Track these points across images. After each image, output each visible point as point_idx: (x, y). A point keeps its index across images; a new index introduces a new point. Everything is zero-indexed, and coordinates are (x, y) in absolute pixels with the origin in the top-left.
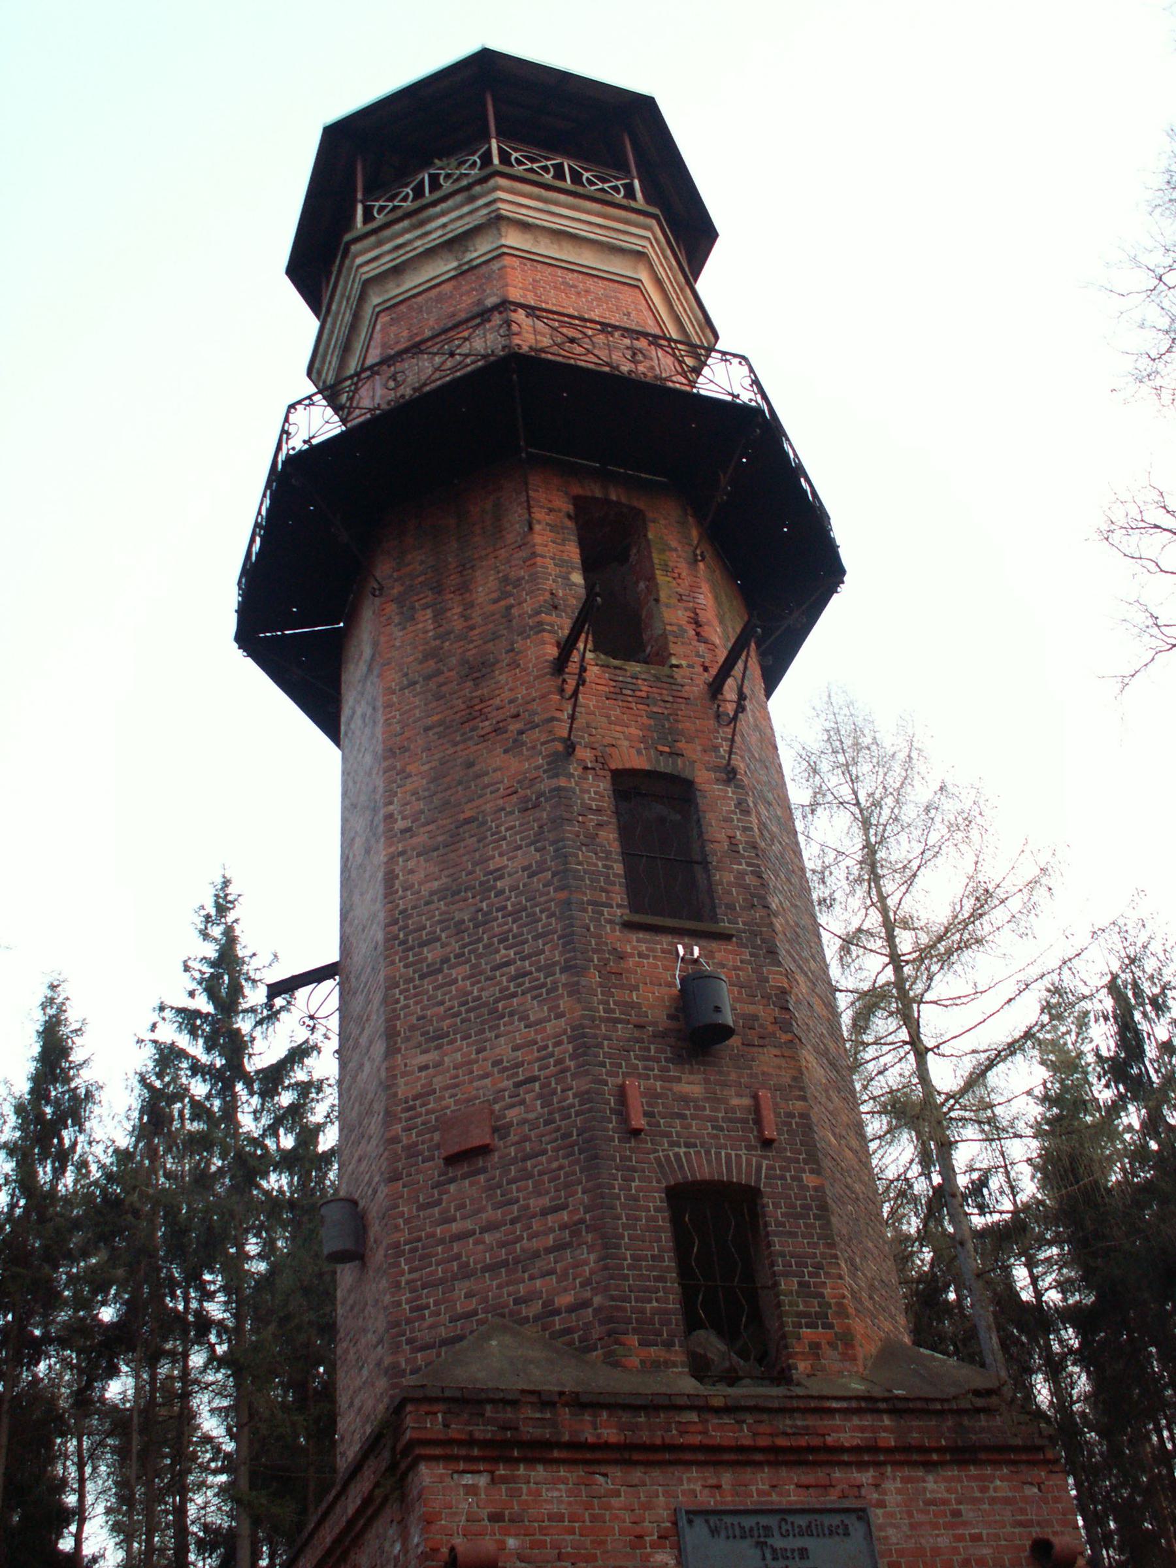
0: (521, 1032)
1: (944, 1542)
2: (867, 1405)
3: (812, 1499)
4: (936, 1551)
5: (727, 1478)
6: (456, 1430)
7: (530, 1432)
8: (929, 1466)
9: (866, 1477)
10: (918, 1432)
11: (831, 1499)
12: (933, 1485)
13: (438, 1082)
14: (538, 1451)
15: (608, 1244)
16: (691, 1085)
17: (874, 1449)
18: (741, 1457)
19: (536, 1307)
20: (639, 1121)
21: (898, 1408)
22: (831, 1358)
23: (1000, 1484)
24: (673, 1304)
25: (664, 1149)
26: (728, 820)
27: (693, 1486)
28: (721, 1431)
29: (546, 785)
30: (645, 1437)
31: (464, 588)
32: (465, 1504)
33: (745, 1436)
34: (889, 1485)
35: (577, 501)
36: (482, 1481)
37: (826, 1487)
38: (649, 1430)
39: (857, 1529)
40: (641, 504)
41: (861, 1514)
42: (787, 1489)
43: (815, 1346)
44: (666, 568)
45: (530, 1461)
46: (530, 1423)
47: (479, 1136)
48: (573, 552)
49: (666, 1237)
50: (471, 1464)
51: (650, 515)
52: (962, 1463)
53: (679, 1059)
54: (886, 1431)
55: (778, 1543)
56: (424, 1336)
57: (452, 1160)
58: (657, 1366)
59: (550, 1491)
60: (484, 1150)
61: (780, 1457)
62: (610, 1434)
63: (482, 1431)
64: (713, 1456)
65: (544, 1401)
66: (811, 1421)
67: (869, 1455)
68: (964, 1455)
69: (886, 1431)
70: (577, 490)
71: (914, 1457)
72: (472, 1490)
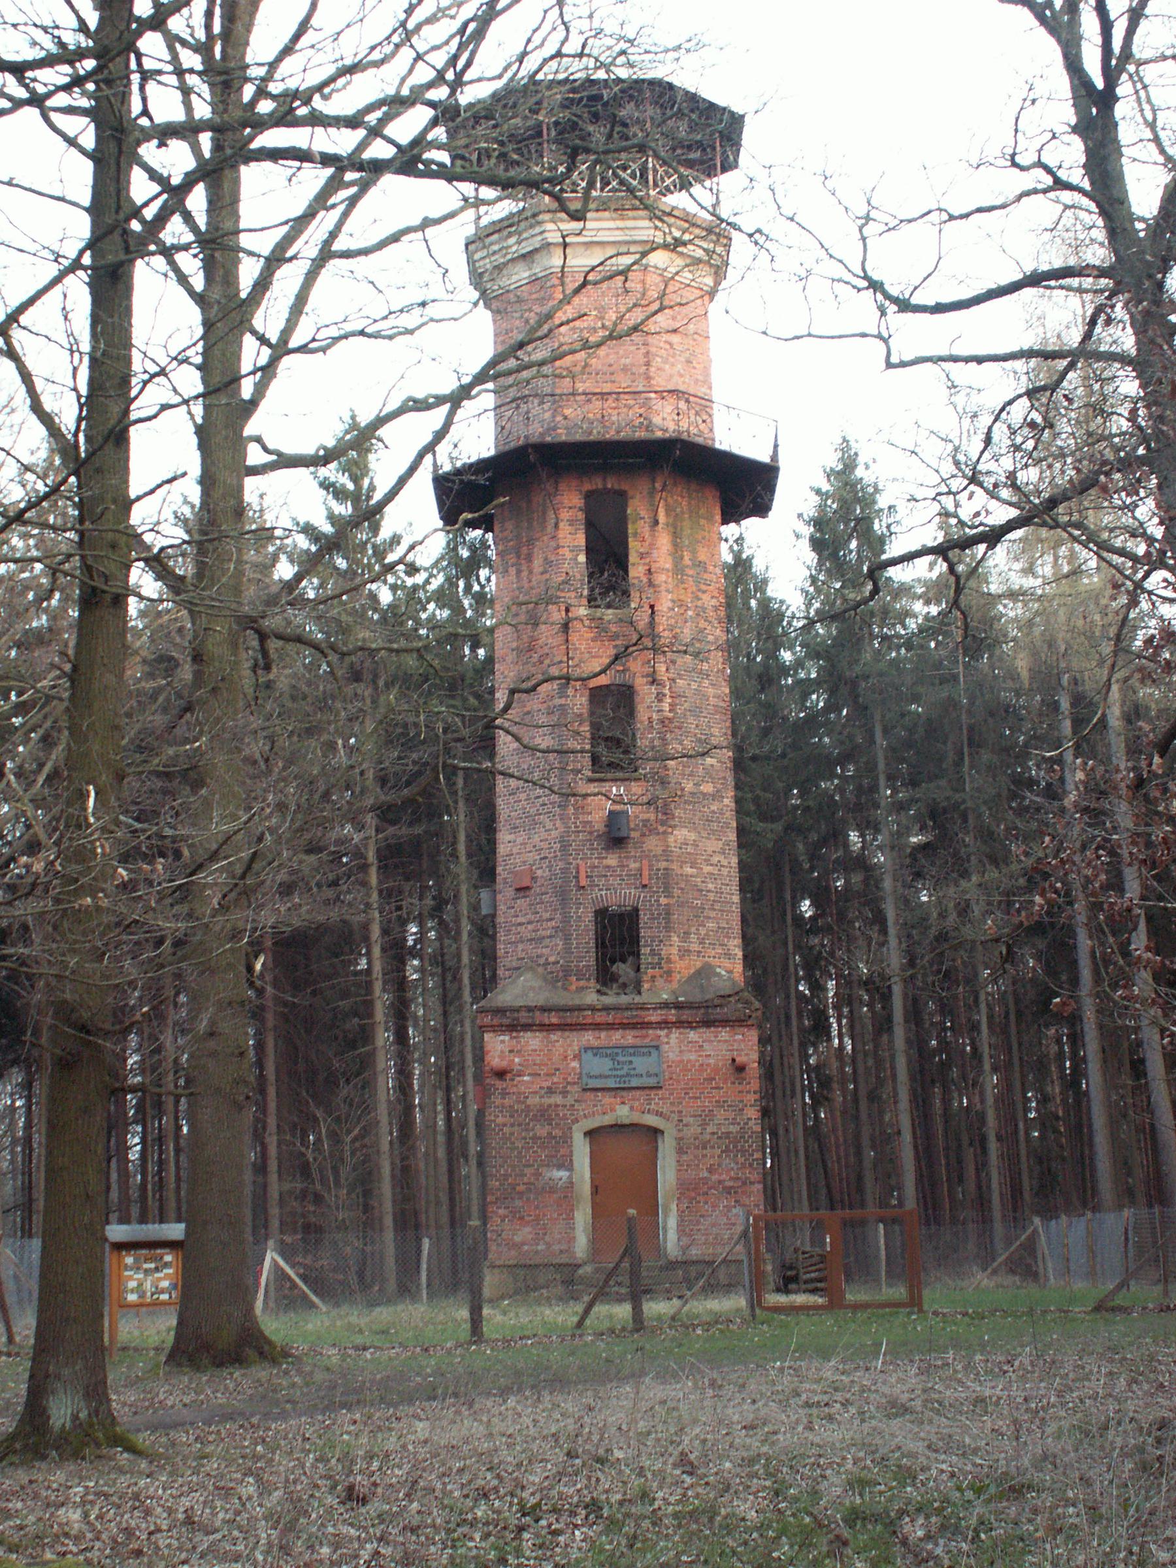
0: (544, 835)
1: (693, 1057)
2: (665, 1005)
3: (638, 1042)
4: (689, 1061)
5: (603, 1034)
6: (495, 1022)
7: (523, 1021)
8: (692, 1028)
9: (663, 1033)
10: (686, 1015)
11: (647, 1041)
12: (692, 1035)
13: (515, 851)
14: (527, 1027)
15: (567, 938)
16: (612, 860)
17: (666, 1022)
18: (610, 1027)
19: (542, 961)
20: (583, 883)
21: (678, 1006)
22: (660, 982)
23: (724, 1034)
24: (593, 962)
25: (596, 893)
26: (649, 707)
27: (589, 1037)
28: (600, 1018)
29: (558, 701)
30: (569, 1021)
31: (529, 558)
32: (499, 1047)
33: (610, 1019)
34: (673, 1036)
35: (588, 496)
36: (507, 1038)
37: (646, 1036)
38: (570, 1018)
39: (654, 1053)
40: (624, 486)
41: (657, 1047)
42: (630, 1038)
43: (653, 977)
44: (635, 534)
45: (526, 1031)
46: (524, 1017)
47: (526, 882)
48: (581, 539)
49: (592, 934)
50: (503, 1032)
51: (630, 493)
52: (708, 1027)
53: (607, 848)
54: (672, 1015)
55: (620, 1058)
56: (508, 965)
57: (518, 890)
58: (581, 989)
59: (532, 1041)
60: (528, 888)
61: (624, 1026)
62: (554, 1020)
63: (506, 1021)
64: (597, 1027)
65: (530, 1009)
66: (639, 1012)
67: (664, 1024)
68: (708, 1023)
69: (672, 1015)
70: (587, 487)
71: (680, 1024)
72: (503, 1042)
